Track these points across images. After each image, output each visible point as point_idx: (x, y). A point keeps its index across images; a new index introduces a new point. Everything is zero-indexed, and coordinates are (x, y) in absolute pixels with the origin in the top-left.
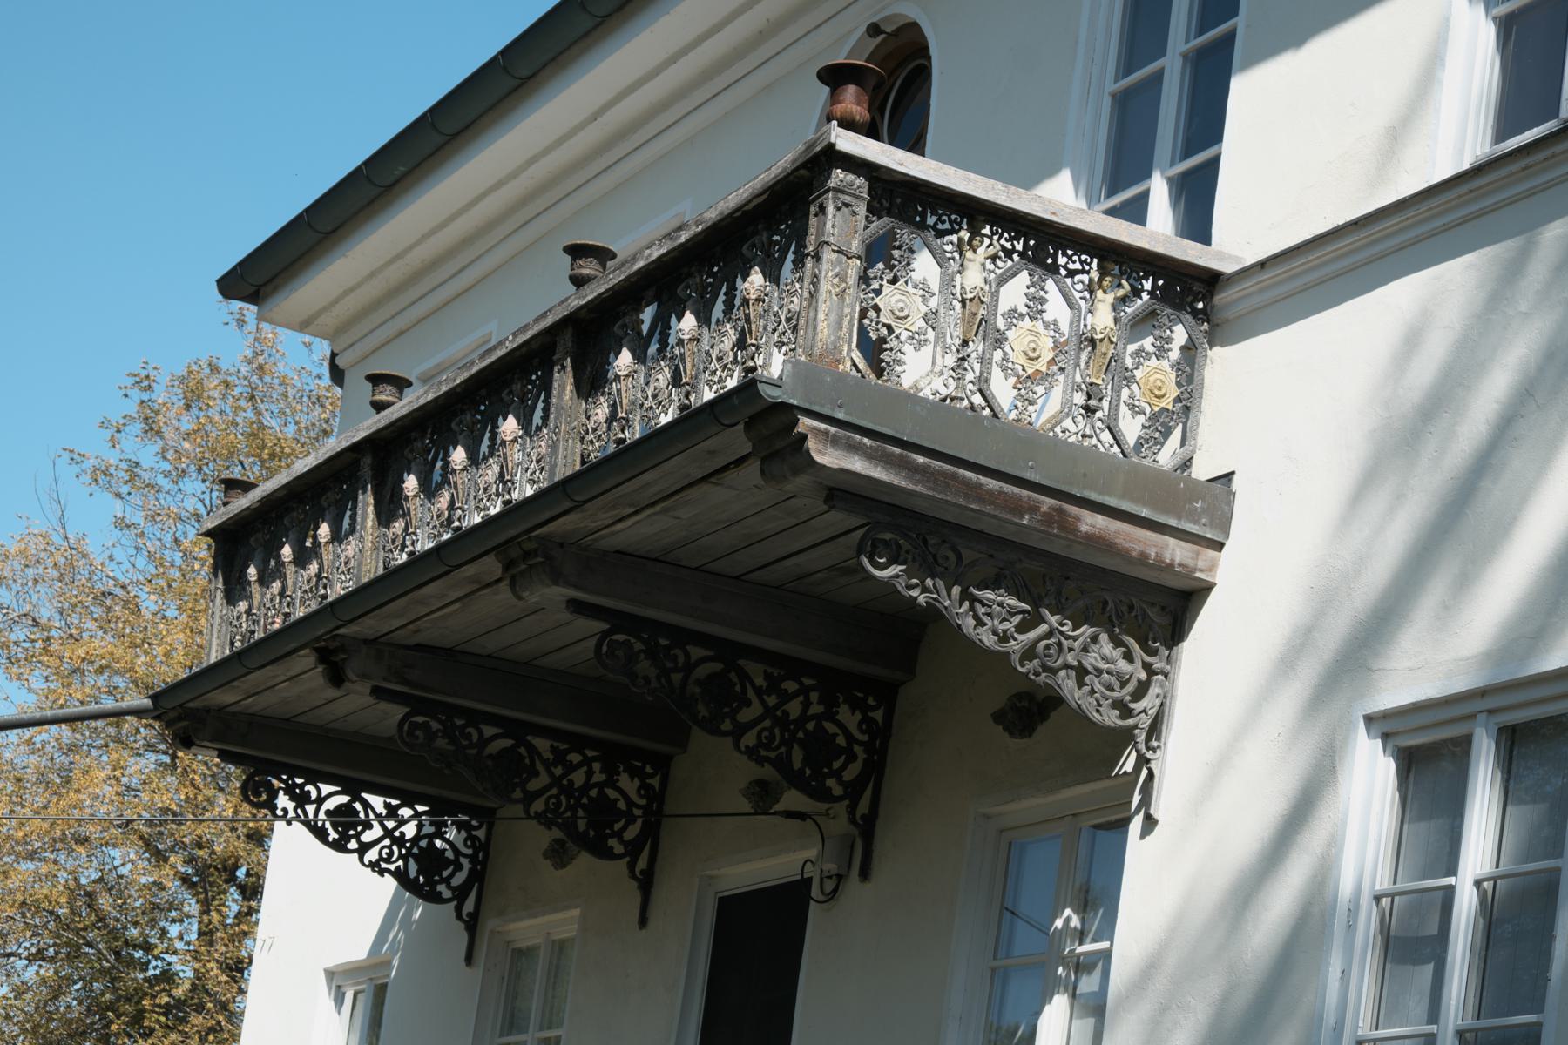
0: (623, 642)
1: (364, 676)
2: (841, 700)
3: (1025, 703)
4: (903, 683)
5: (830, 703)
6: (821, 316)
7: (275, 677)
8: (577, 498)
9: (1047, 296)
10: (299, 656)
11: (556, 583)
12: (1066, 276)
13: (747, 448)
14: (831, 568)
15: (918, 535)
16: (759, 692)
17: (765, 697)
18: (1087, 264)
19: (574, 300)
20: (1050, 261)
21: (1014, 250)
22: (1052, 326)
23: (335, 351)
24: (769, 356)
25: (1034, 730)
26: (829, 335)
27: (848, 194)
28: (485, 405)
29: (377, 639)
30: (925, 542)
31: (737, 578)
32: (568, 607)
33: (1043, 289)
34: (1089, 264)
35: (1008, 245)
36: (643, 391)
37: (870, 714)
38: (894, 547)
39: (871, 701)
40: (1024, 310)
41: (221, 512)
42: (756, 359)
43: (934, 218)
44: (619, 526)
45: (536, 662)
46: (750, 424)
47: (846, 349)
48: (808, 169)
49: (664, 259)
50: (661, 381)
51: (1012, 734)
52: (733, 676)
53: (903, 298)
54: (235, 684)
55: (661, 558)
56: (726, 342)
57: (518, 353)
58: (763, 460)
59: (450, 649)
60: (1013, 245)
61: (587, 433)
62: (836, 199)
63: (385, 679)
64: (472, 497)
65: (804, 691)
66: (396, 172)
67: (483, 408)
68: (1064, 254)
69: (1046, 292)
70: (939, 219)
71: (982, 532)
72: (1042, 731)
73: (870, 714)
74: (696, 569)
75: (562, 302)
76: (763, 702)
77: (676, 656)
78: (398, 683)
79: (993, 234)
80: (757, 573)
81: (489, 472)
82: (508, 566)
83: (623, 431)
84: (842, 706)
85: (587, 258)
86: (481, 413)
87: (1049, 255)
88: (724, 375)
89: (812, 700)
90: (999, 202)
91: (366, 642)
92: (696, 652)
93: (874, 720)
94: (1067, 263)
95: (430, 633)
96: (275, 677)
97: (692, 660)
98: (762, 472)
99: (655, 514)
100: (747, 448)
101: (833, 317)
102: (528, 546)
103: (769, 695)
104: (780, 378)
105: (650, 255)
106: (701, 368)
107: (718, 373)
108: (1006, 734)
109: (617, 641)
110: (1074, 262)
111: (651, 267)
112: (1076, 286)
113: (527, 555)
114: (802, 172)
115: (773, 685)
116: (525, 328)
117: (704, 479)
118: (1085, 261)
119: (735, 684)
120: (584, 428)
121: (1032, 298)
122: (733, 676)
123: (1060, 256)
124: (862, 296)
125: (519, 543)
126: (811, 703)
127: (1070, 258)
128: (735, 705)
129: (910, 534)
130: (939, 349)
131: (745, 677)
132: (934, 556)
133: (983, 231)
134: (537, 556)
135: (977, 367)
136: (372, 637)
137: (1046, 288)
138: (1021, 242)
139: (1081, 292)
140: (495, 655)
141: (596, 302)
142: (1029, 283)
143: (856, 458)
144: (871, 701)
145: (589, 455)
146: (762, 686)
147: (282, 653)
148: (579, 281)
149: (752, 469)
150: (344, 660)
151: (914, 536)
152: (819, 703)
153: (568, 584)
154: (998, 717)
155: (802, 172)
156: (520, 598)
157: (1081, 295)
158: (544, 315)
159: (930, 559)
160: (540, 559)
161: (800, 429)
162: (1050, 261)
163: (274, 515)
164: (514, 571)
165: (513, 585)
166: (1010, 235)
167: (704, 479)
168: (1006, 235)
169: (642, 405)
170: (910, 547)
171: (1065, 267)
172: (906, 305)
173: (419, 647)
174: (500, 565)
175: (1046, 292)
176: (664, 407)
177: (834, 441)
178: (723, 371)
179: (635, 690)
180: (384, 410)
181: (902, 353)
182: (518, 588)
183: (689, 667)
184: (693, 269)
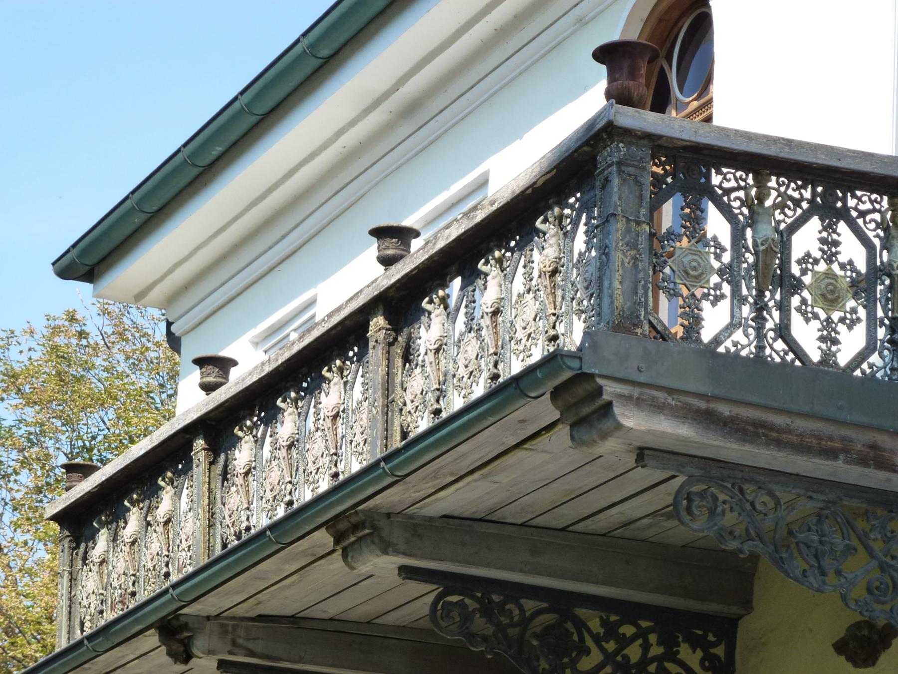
0: (456, 603)
1: (210, 652)
2: (680, 639)
3: (866, 632)
4: (741, 617)
5: (670, 644)
6: (617, 285)
7: (123, 656)
8: (399, 473)
9: (840, 239)
10: (146, 636)
11: (385, 552)
12: (858, 217)
13: (556, 415)
14: (654, 514)
15: (733, 485)
16: (597, 639)
17: (603, 643)
18: (877, 203)
19: (383, 280)
20: (839, 204)
21: (802, 199)
22: (848, 267)
23: (170, 320)
24: (570, 325)
25: (877, 659)
26: (625, 301)
27: (633, 166)
28: (306, 381)
29: (218, 615)
30: (741, 491)
31: (563, 529)
32: (399, 574)
33: (835, 231)
34: (879, 203)
35: (796, 195)
36: (455, 362)
37: (712, 651)
38: (710, 499)
39: (711, 638)
40: (818, 255)
41: (64, 496)
42: (557, 327)
43: (720, 177)
44: (441, 494)
45: (376, 621)
46: (556, 394)
47: (643, 313)
48: (592, 146)
49: (462, 238)
50: (470, 352)
51: (856, 665)
52: (569, 625)
53: (696, 257)
54: (86, 666)
55: (487, 518)
56: (528, 312)
57: (333, 332)
58: (572, 426)
59: (293, 616)
60: (801, 194)
61: (405, 404)
62: (620, 172)
63: (230, 653)
64: (301, 471)
65: (642, 634)
66: (213, 153)
67: (305, 385)
68: (854, 196)
69: (839, 235)
70: (725, 178)
71: (798, 475)
72: (884, 659)
73: (712, 651)
74: (522, 525)
75: (372, 283)
76: (602, 650)
77: (510, 611)
78: (246, 656)
79: (779, 185)
80: (588, 522)
81: (316, 446)
82: (337, 541)
83: (438, 401)
84: (682, 645)
85: (392, 238)
86: (305, 390)
87: (838, 199)
88: (528, 344)
89: (651, 642)
90: (782, 155)
91: (208, 618)
92: (530, 605)
93: (716, 657)
94: (858, 204)
95: (273, 605)
96: (123, 656)
97: (528, 614)
98: (572, 438)
99: (475, 481)
100: (556, 415)
101: (627, 284)
102: (354, 519)
103: (607, 642)
104: (580, 349)
105: (449, 235)
106: (507, 338)
107: (523, 342)
108: (849, 664)
109: (451, 602)
110: (864, 203)
111: (452, 245)
112: (868, 226)
113: (356, 527)
114: (585, 148)
115: (611, 631)
116: (338, 310)
117: (518, 446)
118: (876, 201)
119: (573, 633)
120: (402, 400)
121: (823, 241)
122: (569, 625)
123: (849, 198)
124: (654, 260)
125: (347, 517)
126: (652, 645)
127: (859, 199)
128: (574, 654)
129: (725, 484)
130: (735, 302)
131: (581, 625)
132: (752, 504)
133: (769, 184)
134: (364, 528)
135: (776, 314)
136: (216, 614)
137: (838, 230)
138: (809, 189)
139: (874, 230)
140: (336, 618)
141: (403, 281)
142: (821, 228)
143: (663, 418)
144: (711, 638)
145: (409, 426)
146: (598, 633)
147: (129, 635)
148: (387, 261)
149: (563, 432)
150: (190, 638)
151: (729, 486)
152: (659, 644)
153: (397, 552)
154: (840, 647)
155: (585, 148)
156: (352, 568)
157: (874, 233)
158: (357, 295)
159: (748, 506)
160: (367, 531)
161: (606, 397)
162: (839, 204)
163: (115, 496)
164: (345, 543)
165: (345, 556)
166: (796, 184)
167: (518, 446)
168: (793, 185)
169: (454, 376)
170: (727, 498)
171: (856, 209)
172: (699, 264)
173: (262, 618)
174: (332, 539)
175: (839, 235)
176: (475, 376)
177: (638, 403)
178: (528, 340)
179: (473, 649)
180: (214, 390)
181: (699, 310)
182: (349, 559)
183: (525, 621)
184: (492, 244)
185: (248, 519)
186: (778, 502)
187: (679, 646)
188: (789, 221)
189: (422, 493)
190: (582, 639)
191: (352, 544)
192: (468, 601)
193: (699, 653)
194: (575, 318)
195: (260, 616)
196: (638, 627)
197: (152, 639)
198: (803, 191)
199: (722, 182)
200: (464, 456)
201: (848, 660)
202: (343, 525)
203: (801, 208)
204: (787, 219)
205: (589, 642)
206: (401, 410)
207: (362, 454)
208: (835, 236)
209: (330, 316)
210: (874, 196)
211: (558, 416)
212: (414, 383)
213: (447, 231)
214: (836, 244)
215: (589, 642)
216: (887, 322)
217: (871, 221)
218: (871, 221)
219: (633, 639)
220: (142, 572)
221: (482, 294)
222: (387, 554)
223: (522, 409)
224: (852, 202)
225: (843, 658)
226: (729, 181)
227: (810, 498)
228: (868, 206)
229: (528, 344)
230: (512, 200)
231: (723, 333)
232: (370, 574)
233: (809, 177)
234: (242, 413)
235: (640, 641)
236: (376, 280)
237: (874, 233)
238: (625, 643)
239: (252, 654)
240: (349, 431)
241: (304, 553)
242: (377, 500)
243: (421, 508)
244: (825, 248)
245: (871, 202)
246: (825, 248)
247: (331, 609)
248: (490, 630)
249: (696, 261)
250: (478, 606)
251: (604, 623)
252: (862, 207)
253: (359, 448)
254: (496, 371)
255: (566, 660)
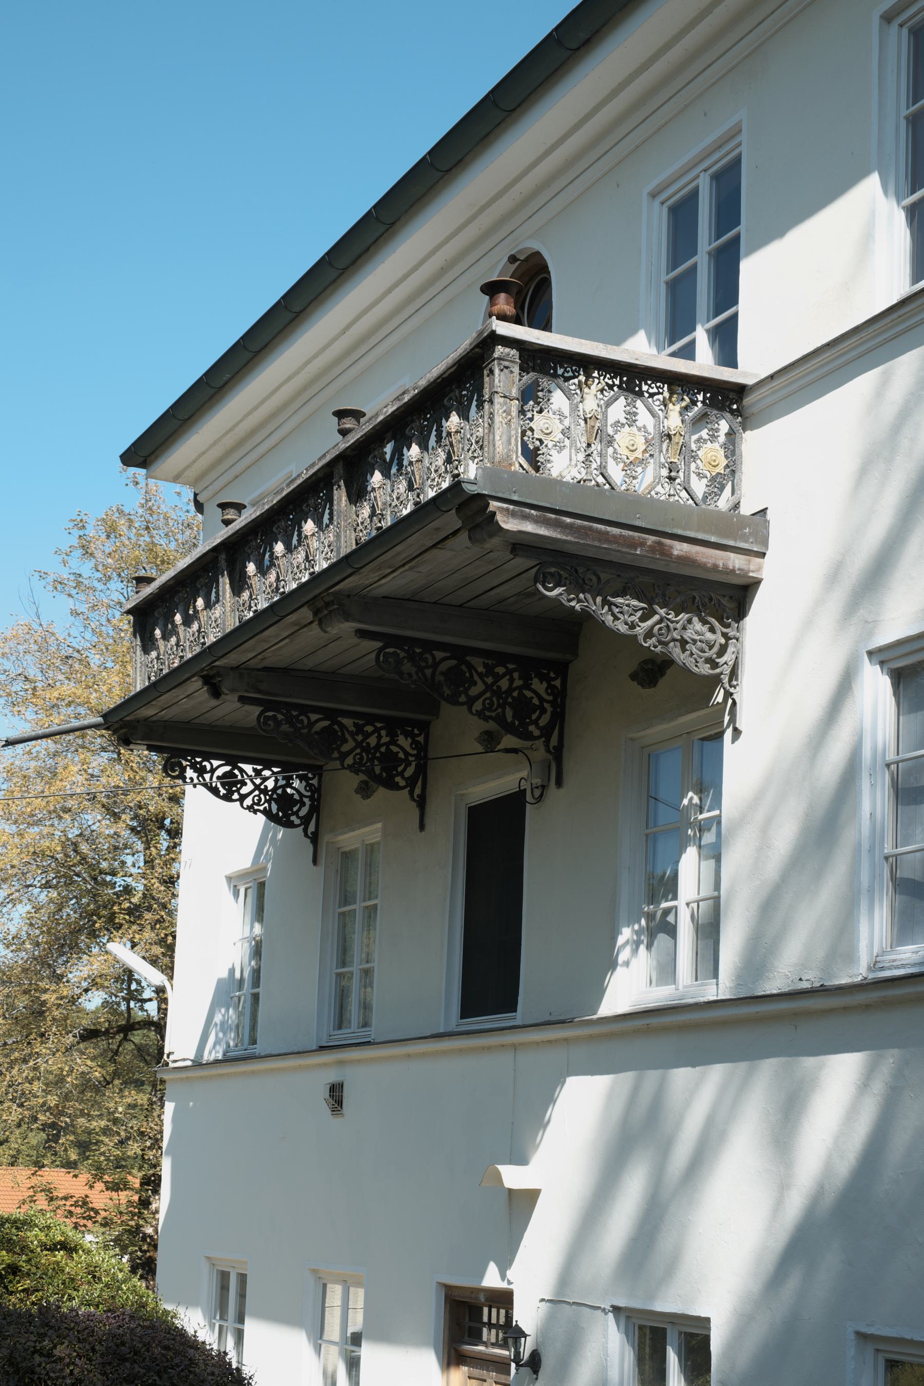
1: (233, 690)
3: (650, 666)
5: (526, 678)
7: (177, 696)
8: (356, 566)
12: (649, 397)
13: (459, 524)
14: (518, 594)
16: (481, 675)
17: (485, 679)
21: (614, 385)
24: (467, 466)
29: (238, 667)
30: (576, 571)
31: (460, 606)
34: (662, 388)
37: (552, 683)
39: (552, 675)
43: (562, 370)
44: (383, 581)
45: (338, 672)
46: (458, 510)
52: (463, 667)
54: (153, 703)
58: (470, 530)
59: (285, 668)
60: (613, 381)
61: (358, 525)
63: (246, 691)
64: (290, 572)
65: (509, 672)
68: (646, 384)
70: (565, 370)
72: (662, 682)
73: (552, 683)
74: (434, 603)
75: (335, 446)
76: (485, 683)
77: (427, 658)
79: (600, 376)
82: (316, 613)
87: (636, 385)
88: (440, 481)
92: (439, 655)
93: (555, 687)
96: (177, 696)
98: (470, 538)
100: (459, 524)
101: (505, 438)
103: (488, 677)
105: (386, 412)
106: (425, 478)
107: (436, 480)
108: (640, 687)
110: (653, 388)
113: (328, 604)
115: (490, 670)
122: (463, 667)
124: (522, 423)
127: (650, 386)
131: (471, 667)
132: (583, 579)
133: (594, 375)
134: (333, 604)
135: (598, 459)
137: (637, 406)
138: (618, 379)
142: (625, 404)
143: (528, 523)
149: (464, 536)
152: (520, 679)
153: (354, 620)
154: (634, 677)
155: (477, 350)
156: (325, 632)
157: (659, 408)
158: (324, 455)
159: (581, 581)
160: (336, 607)
164: (321, 615)
165: (320, 624)
171: (647, 392)
173: (265, 669)
177: (513, 514)
185: (256, 606)
186: (599, 579)
187: (532, 680)
188: (606, 399)
189: (371, 580)
190: (471, 676)
191: (325, 616)
192: (399, 651)
193: (545, 685)
194: (471, 462)
195: (265, 668)
196: (507, 668)
197: (196, 684)
198: (614, 380)
199: (563, 373)
200: (399, 553)
201: (638, 684)
202: (320, 604)
203: (614, 391)
204: (605, 398)
205: (476, 678)
206: (355, 529)
207: (330, 559)
208: (634, 409)
209: (320, 459)
210: (658, 384)
211: (461, 525)
212: (364, 511)
213: (385, 409)
214: (635, 414)
215: (476, 678)
216: (666, 465)
217: (657, 400)
218: (657, 400)
219: (504, 675)
220: (188, 643)
221: (409, 450)
222: (348, 621)
223: (438, 520)
224: (645, 388)
225: (635, 683)
226: (568, 372)
227: (619, 576)
228: (655, 390)
229: (440, 481)
230: (428, 386)
231: (68, 1104)
232: (339, 636)
233: (619, 371)
234: (250, 538)
235: (508, 677)
236: (337, 444)
237: (659, 408)
238: (498, 677)
239: (259, 691)
240: (321, 545)
241: (294, 624)
242: (341, 586)
243: (374, 589)
244: (628, 417)
245: (657, 388)
246: (628, 417)
247: (310, 663)
248: (413, 670)
249: (547, 423)
250: (406, 655)
251: (485, 666)
252: (651, 391)
253: (328, 556)
254: (418, 500)
255: (461, 689)
